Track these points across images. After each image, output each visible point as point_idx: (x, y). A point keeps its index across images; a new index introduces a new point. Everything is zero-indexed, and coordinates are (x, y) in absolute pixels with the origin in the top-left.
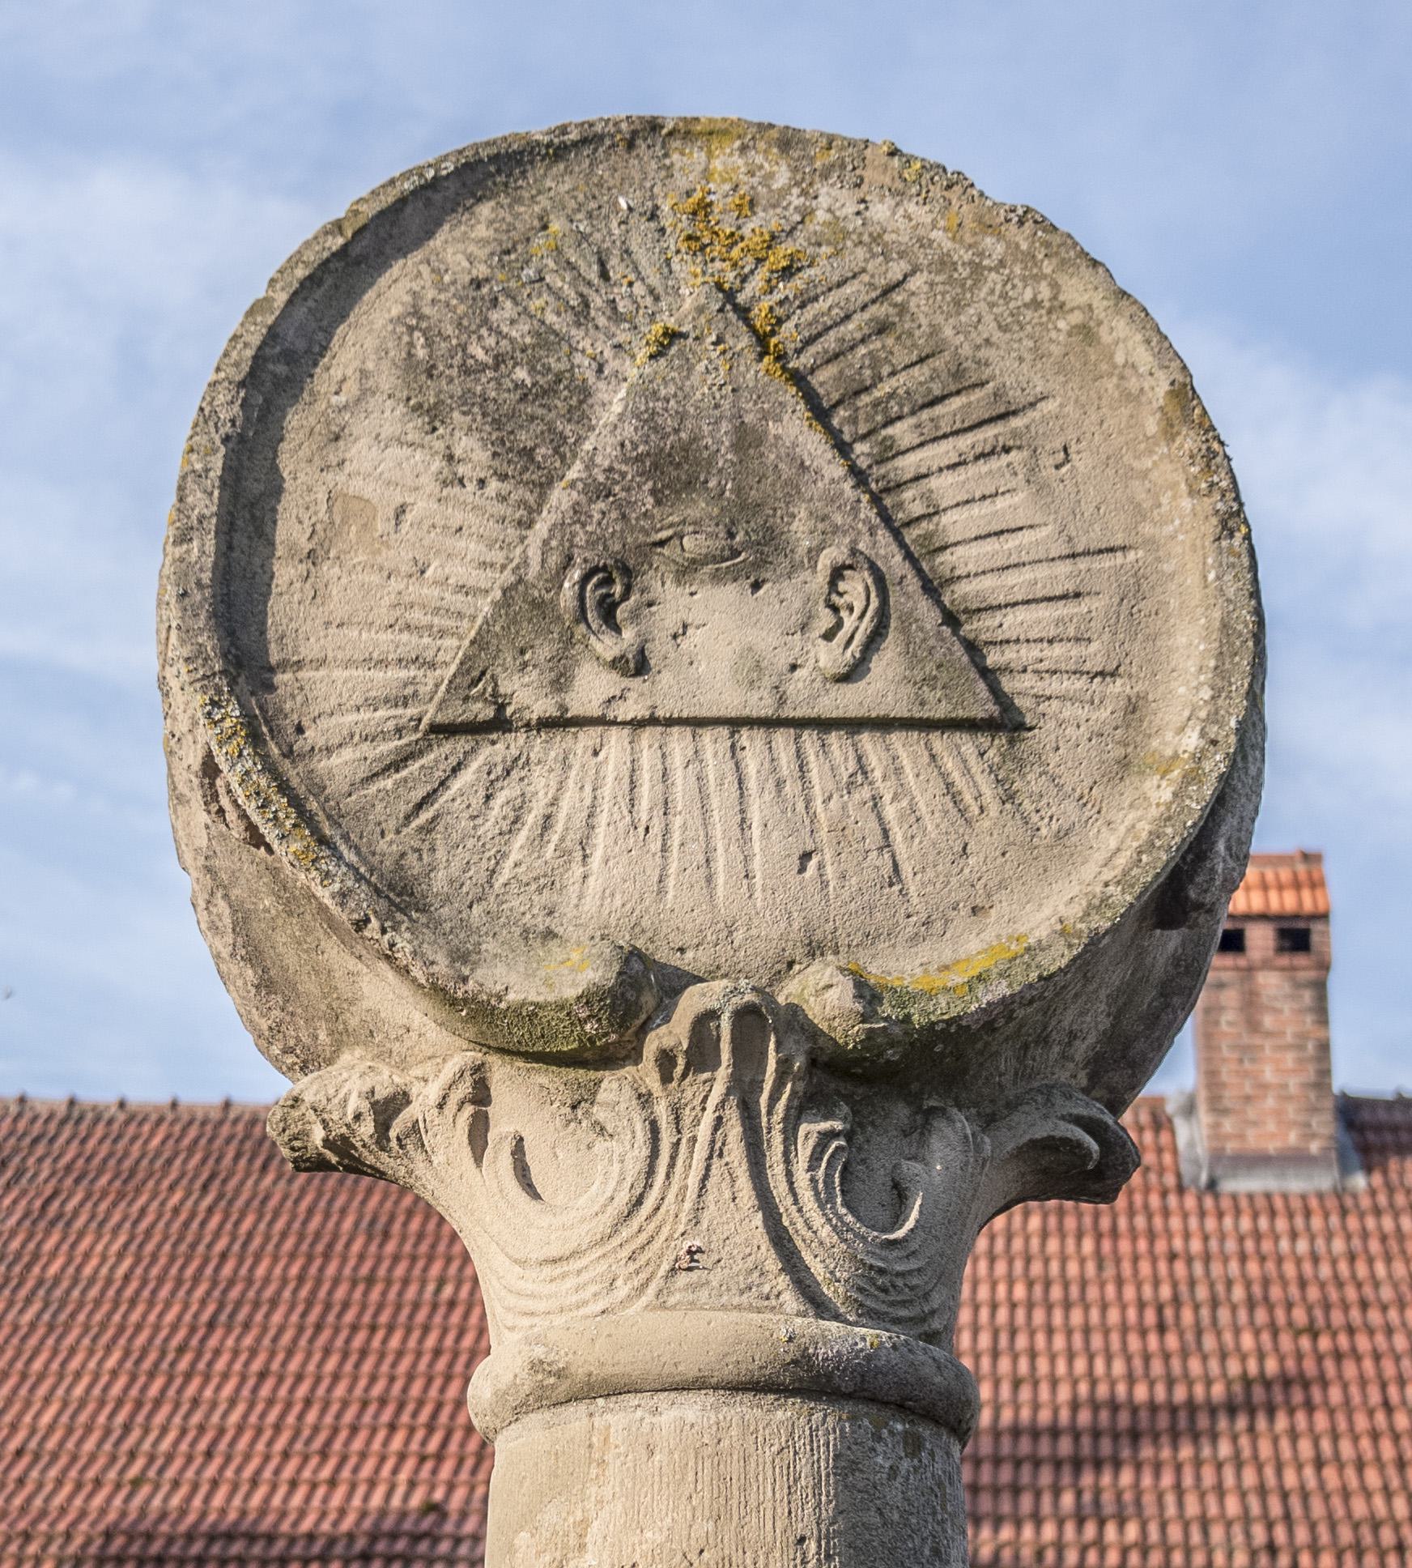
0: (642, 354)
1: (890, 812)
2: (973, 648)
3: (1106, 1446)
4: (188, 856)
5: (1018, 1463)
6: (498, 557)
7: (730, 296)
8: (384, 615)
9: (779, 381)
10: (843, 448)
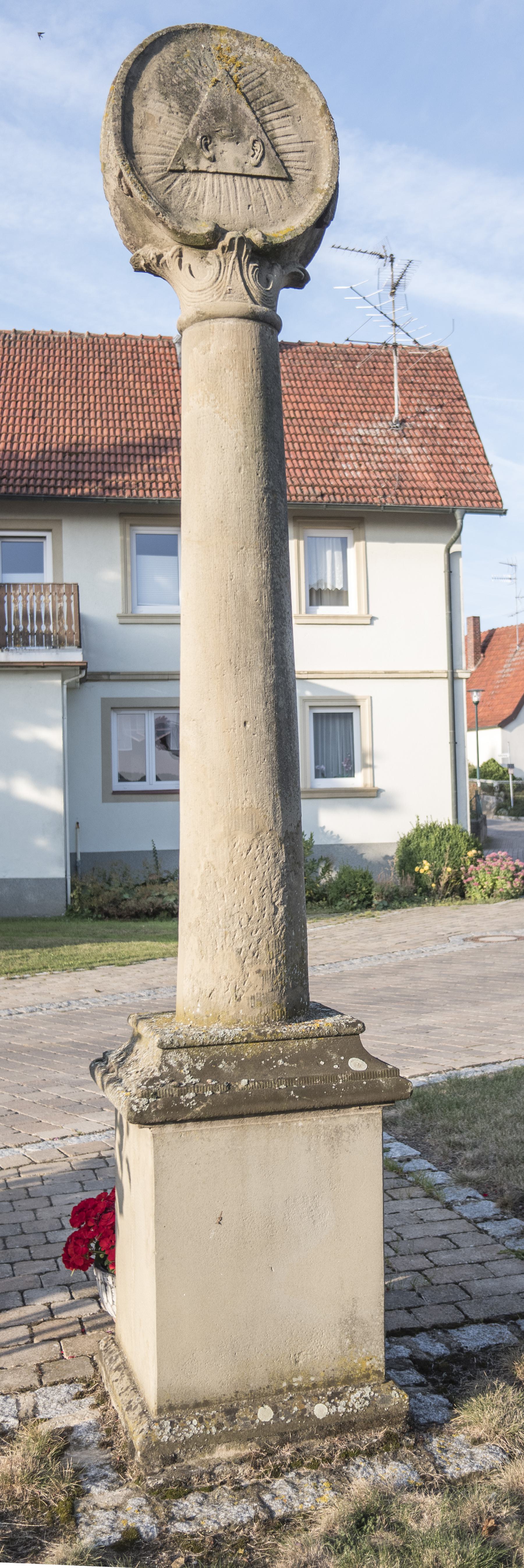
0: (210, 85)
1: (266, 197)
2: (282, 161)
3: (157, 451)
4: (109, 198)
5: (129, 456)
6: (181, 131)
7: (228, 72)
8: (158, 143)
9: (240, 94)
10: (254, 112)
